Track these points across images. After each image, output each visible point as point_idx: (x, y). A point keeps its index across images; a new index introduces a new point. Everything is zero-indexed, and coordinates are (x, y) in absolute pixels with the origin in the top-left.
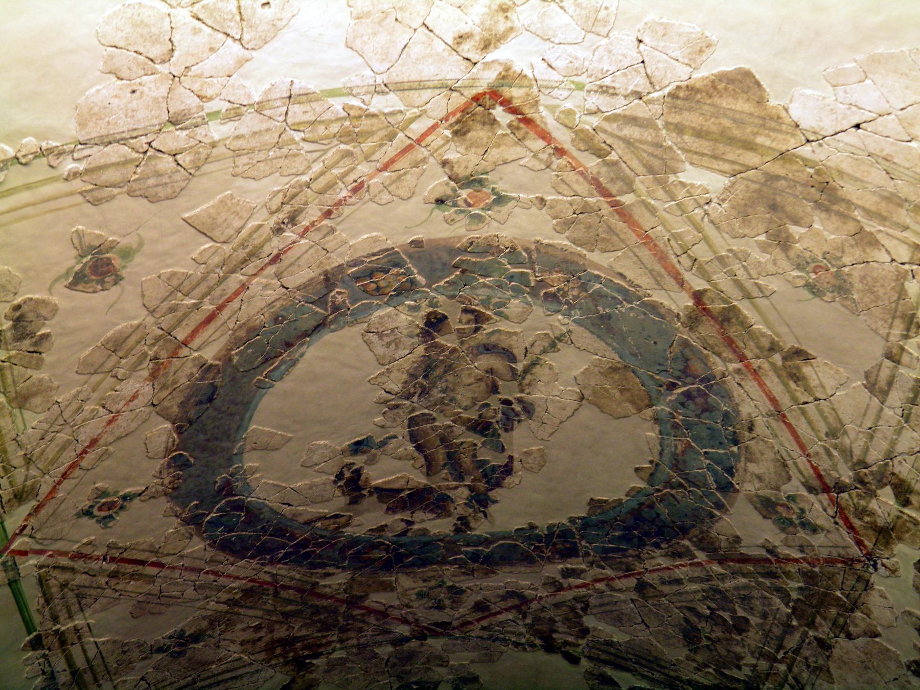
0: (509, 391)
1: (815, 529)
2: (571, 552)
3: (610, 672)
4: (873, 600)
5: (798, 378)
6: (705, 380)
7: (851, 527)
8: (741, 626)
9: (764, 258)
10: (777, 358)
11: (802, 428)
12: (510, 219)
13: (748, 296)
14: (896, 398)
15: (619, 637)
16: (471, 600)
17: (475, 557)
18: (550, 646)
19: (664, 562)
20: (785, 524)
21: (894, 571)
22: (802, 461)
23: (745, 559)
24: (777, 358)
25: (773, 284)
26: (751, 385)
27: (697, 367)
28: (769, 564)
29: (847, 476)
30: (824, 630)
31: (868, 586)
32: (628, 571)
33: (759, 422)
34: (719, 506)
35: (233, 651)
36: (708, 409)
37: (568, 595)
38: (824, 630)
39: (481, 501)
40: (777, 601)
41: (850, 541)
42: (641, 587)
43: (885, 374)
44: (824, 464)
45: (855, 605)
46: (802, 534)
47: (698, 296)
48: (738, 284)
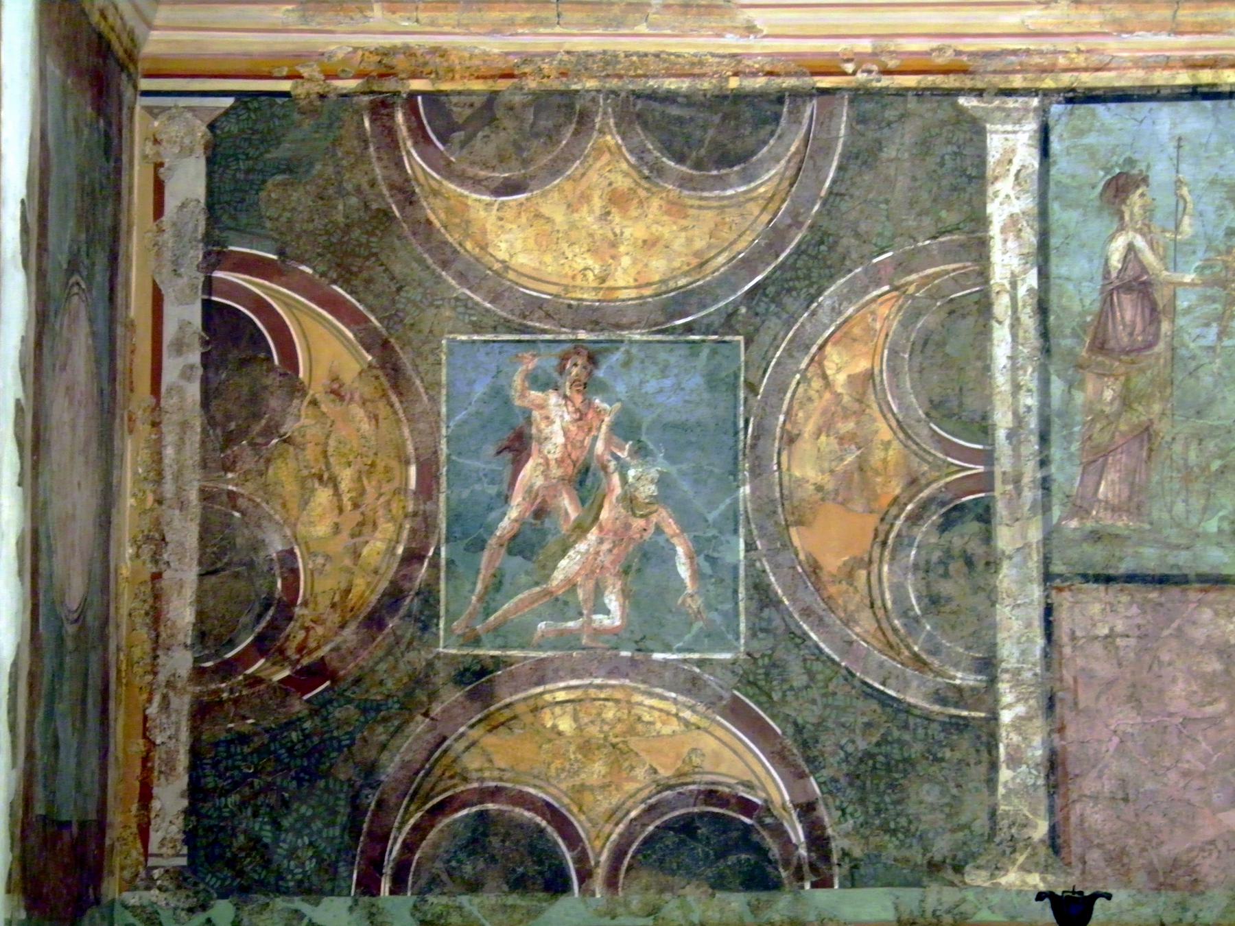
12: (1058, 268)
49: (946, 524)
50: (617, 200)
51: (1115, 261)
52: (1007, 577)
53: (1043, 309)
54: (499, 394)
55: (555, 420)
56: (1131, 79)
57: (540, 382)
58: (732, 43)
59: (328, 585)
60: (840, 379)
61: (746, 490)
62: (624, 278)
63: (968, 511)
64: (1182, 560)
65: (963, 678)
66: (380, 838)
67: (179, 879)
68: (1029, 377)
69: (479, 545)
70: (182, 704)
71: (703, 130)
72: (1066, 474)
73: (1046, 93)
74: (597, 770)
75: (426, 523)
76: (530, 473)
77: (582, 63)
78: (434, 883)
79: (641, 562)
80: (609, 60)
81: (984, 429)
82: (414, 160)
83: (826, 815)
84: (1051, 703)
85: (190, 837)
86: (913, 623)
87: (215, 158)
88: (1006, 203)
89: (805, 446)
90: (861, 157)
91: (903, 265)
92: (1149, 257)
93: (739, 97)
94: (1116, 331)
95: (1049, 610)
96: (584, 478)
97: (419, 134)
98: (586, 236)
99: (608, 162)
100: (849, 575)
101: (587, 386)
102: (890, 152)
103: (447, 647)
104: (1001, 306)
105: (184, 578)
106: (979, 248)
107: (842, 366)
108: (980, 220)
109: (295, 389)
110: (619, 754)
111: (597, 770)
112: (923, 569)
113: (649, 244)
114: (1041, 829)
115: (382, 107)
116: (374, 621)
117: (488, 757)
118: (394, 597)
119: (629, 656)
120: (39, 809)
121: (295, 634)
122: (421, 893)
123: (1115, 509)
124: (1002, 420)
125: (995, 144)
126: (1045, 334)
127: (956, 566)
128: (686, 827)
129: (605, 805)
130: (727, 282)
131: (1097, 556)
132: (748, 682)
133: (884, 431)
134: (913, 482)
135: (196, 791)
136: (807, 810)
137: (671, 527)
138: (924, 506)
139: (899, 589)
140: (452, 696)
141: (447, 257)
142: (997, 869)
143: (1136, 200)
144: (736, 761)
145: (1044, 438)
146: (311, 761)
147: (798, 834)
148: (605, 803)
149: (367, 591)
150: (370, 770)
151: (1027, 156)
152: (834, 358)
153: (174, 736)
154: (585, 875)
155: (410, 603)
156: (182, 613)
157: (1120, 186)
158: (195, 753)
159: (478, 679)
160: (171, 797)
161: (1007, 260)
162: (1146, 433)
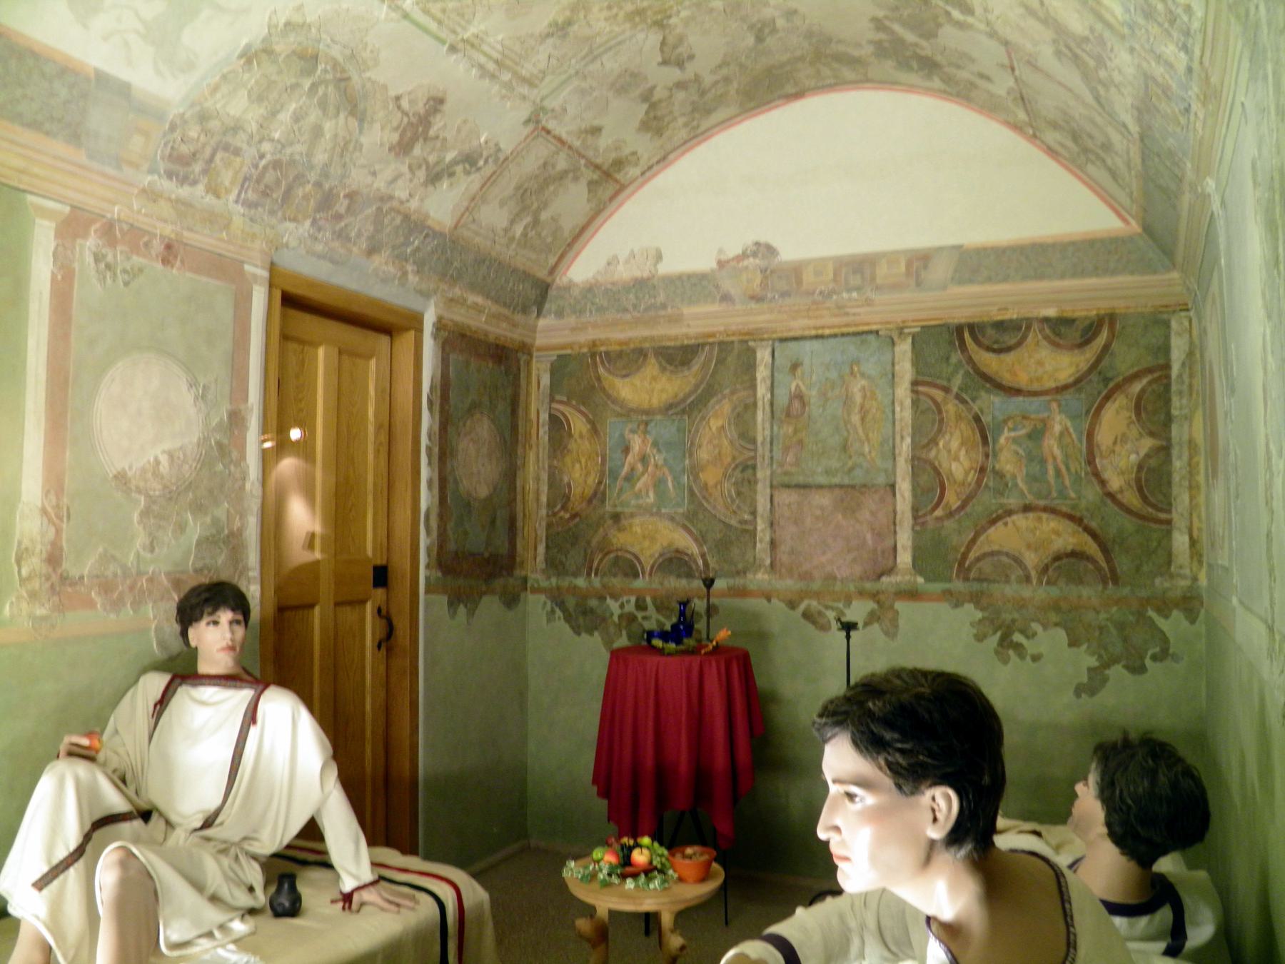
12: (776, 391)
49: (743, 471)
50: (654, 378)
51: (793, 389)
52: (760, 486)
53: (772, 404)
54: (622, 436)
55: (636, 443)
56: (798, 333)
57: (632, 431)
58: (684, 330)
59: (579, 490)
60: (714, 429)
61: (687, 462)
62: (655, 402)
63: (749, 467)
64: (810, 480)
65: (747, 517)
66: (592, 562)
67: (543, 571)
68: (768, 425)
69: (616, 479)
70: (544, 524)
71: (677, 356)
72: (777, 454)
73: (774, 340)
74: (647, 543)
75: (602, 473)
76: (630, 458)
77: (645, 339)
78: (605, 574)
79: (659, 484)
80: (652, 339)
81: (754, 441)
82: (601, 370)
83: (709, 558)
84: (772, 524)
85: (546, 560)
86: (733, 501)
87: (552, 374)
88: (762, 373)
89: (704, 448)
90: (721, 361)
91: (733, 393)
92: (803, 388)
93: (688, 346)
94: (793, 410)
95: (772, 496)
96: (644, 459)
97: (602, 362)
98: (644, 388)
99: (652, 366)
100: (716, 486)
101: (646, 432)
102: (729, 359)
103: (608, 508)
104: (760, 404)
105: (545, 488)
106: (753, 386)
107: (715, 424)
108: (754, 379)
109: (570, 435)
110: (653, 539)
111: (647, 543)
112: (735, 483)
113: (663, 390)
114: (768, 562)
115: (593, 355)
116: (590, 501)
117: (619, 539)
118: (595, 494)
119: (654, 512)
120: (452, 546)
121: (570, 505)
122: (602, 577)
123: (791, 465)
124: (760, 439)
125: (759, 355)
126: (772, 412)
127: (746, 483)
128: (670, 560)
129: (649, 553)
130: (684, 400)
131: (786, 479)
132: (688, 518)
133: (726, 443)
134: (734, 458)
135: (547, 547)
136: (703, 556)
137: (667, 472)
138: (737, 466)
139: (729, 491)
140: (610, 522)
141: (609, 396)
142: (755, 572)
143: (799, 371)
144: (683, 541)
145: (771, 444)
146: (575, 539)
147: (700, 562)
148: (648, 553)
149: (589, 492)
150: (589, 543)
151: (768, 358)
152: (712, 422)
153: (542, 533)
154: (643, 573)
155: (599, 495)
156: (544, 499)
157: (795, 367)
158: (547, 538)
159: (616, 517)
160: (541, 549)
161: (762, 391)
162: (801, 442)
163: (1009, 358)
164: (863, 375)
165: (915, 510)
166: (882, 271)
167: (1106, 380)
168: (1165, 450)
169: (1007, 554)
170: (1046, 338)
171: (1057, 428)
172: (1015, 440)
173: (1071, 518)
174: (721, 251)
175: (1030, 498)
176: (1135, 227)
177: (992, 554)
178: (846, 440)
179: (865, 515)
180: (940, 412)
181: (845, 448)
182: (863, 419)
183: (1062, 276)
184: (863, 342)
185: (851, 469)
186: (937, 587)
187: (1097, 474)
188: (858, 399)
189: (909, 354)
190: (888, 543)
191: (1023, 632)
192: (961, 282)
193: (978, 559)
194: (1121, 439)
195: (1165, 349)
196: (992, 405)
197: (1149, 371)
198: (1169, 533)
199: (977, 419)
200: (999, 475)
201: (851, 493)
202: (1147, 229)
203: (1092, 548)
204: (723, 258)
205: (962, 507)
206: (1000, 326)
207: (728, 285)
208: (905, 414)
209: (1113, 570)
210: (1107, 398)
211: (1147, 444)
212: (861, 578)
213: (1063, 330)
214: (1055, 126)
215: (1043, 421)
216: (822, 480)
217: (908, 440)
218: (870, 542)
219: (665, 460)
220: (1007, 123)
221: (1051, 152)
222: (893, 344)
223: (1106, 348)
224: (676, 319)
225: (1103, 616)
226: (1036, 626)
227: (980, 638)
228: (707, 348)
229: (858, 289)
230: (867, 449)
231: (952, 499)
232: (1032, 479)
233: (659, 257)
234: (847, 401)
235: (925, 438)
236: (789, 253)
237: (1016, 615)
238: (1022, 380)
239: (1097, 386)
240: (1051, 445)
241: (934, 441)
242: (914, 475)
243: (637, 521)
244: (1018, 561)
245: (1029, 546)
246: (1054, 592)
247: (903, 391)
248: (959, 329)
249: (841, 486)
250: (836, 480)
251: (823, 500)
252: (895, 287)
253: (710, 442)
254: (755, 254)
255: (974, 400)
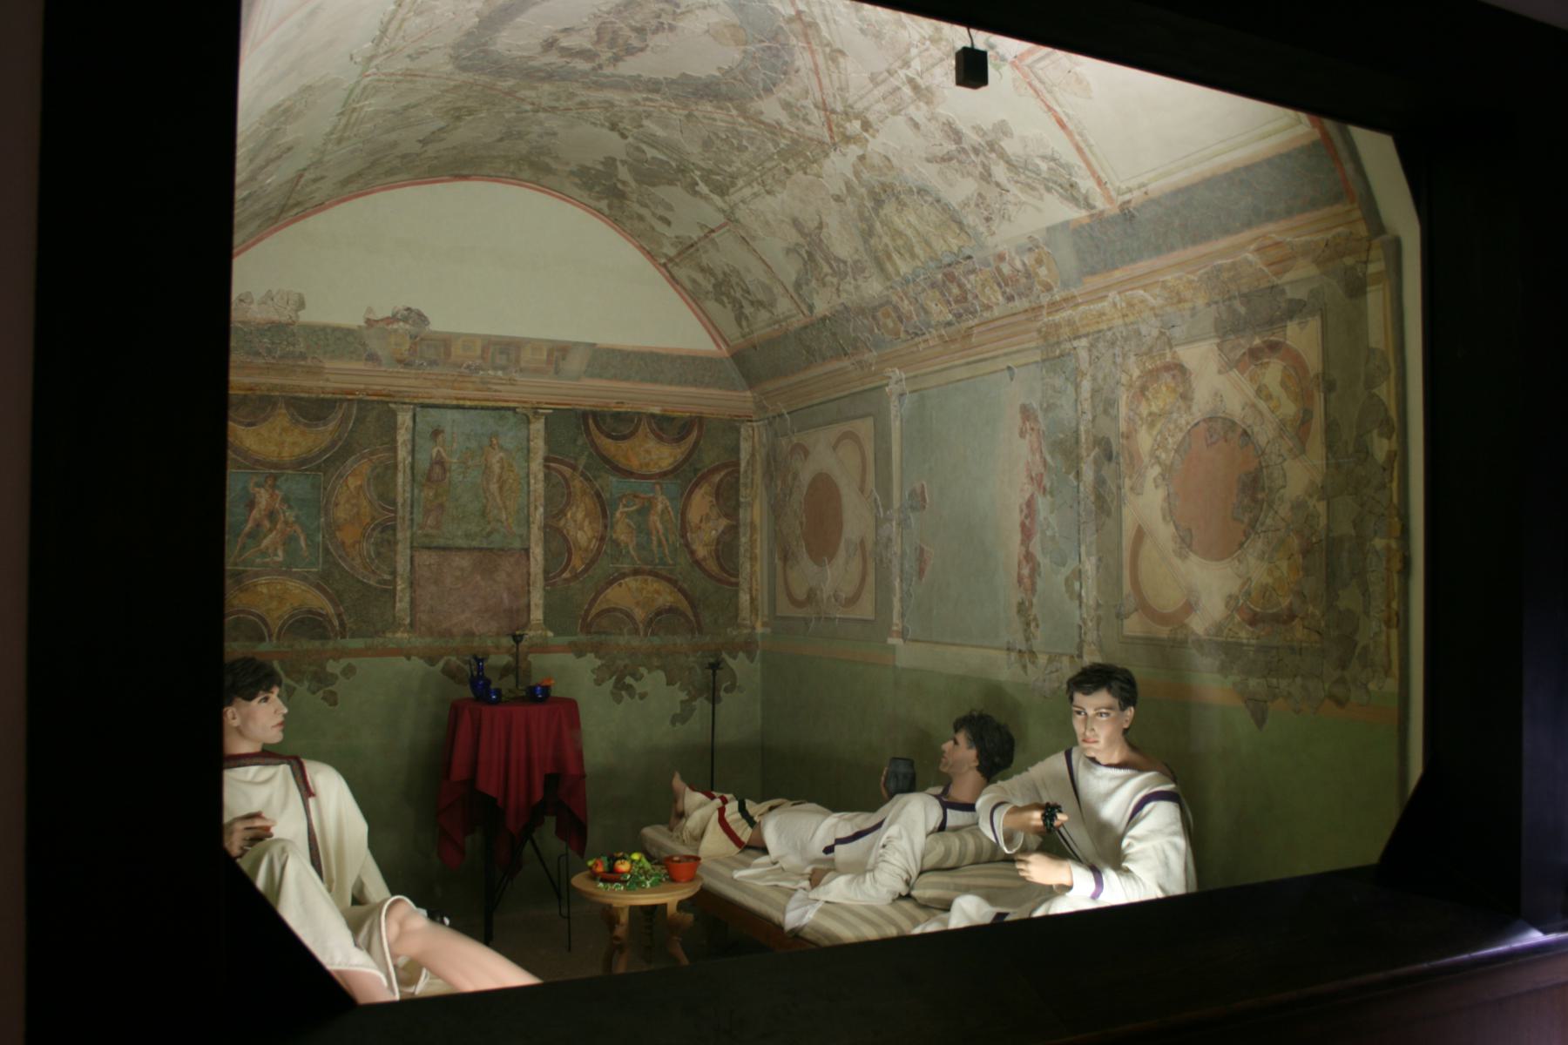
0: (666, 19)
1: (809, 123)
2: (657, 91)
3: (644, 147)
4: (827, 163)
5: (834, 60)
6: (783, 45)
7: (830, 129)
8: (742, 149)
9: (843, 10)
10: (828, 50)
11: (826, 81)
12: (418, 456)
13: (826, 20)
14: (883, 89)
15: (660, 133)
16: (577, 100)
17: (595, 83)
18: (613, 127)
19: (709, 109)
20: (794, 116)
21: (844, 155)
22: (818, 95)
23: (762, 122)
24: (828, 50)
25: (843, 22)
26: (807, 55)
27: (782, 38)
28: (775, 129)
29: (839, 108)
30: (792, 165)
31: (827, 155)
32: (685, 107)
33: (803, 72)
34: (759, 96)
35: (429, 113)
36: (777, 56)
37: (640, 109)
38: (792, 165)
39: (616, 59)
40: (770, 145)
41: (827, 134)
42: (689, 116)
43: (881, 78)
44: (829, 100)
45: (815, 161)
46: (801, 123)
47: (799, 13)
48: (825, 16)
49: (383, 531)
50: (284, 430)
52: (400, 547)
53: (412, 468)
55: (263, 498)
56: (440, 401)
57: (258, 485)
58: (321, 383)
63: (389, 528)
68: (408, 488)
71: (312, 409)
74: (274, 604)
76: (255, 513)
79: (289, 541)
81: (394, 503)
88: (403, 436)
90: (360, 420)
91: (372, 453)
96: (272, 515)
99: (282, 418)
100: (353, 546)
101: (274, 487)
104: (400, 467)
106: (394, 450)
107: (353, 483)
113: (294, 444)
114: (408, 621)
124: (400, 500)
125: (400, 418)
126: (413, 474)
128: (302, 621)
133: (365, 503)
134: (373, 519)
136: (339, 616)
147: (336, 623)
151: (409, 423)
154: (270, 636)
157: (436, 433)
161: (403, 453)
162: (441, 506)
163: (624, 445)
164: (501, 448)
165: (546, 572)
166: (526, 355)
167: (696, 471)
168: (733, 530)
169: (621, 611)
170: (652, 431)
171: (660, 507)
172: (628, 515)
173: (669, 580)
174: (370, 310)
175: (639, 565)
176: (724, 352)
177: (608, 610)
178: (485, 507)
179: (501, 576)
180: (568, 487)
181: (484, 514)
182: (501, 488)
183: (670, 384)
184: (502, 418)
185: (490, 534)
186: (564, 640)
187: (687, 545)
188: (496, 469)
189: (542, 433)
190: (523, 601)
191: (633, 675)
192: (592, 376)
193: (598, 615)
194: (707, 518)
195: (736, 450)
196: (612, 484)
197: (725, 466)
198: (736, 593)
199: (598, 495)
200: (616, 543)
201: (488, 556)
202: (738, 357)
203: (684, 605)
204: (372, 317)
205: (586, 570)
206: (618, 416)
207: (374, 345)
208: (538, 486)
209: (698, 622)
210: (696, 485)
211: (724, 522)
212: (498, 634)
213: (669, 426)
214: (703, 270)
215: (649, 500)
216: (461, 542)
217: (541, 510)
218: (506, 601)
219: (297, 517)
220: (641, 248)
221: (674, 280)
222: (529, 422)
223: (696, 443)
224: (316, 371)
225: (691, 659)
226: (643, 670)
227: (599, 682)
228: (345, 405)
229: (504, 368)
230: (504, 516)
231: (578, 563)
232: (640, 547)
233: (301, 305)
234: (487, 469)
235: (555, 513)
236: (439, 323)
237: (627, 661)
238: (635, 464)
239: (686, 475)
240: (655, 520)
241: (563, 513)
242: (546, 541)
243: (263, 580)
244: (630, 616)
245: (638, 604)
246: (656, 641)
247: (537, 465)
248: (585, 415)
249: (480, 549)
250: (475, 544)
251: (463, 561)
252: (537, 371)
253: (348, 501)
254: (405, 320)
255: (595, 478)
